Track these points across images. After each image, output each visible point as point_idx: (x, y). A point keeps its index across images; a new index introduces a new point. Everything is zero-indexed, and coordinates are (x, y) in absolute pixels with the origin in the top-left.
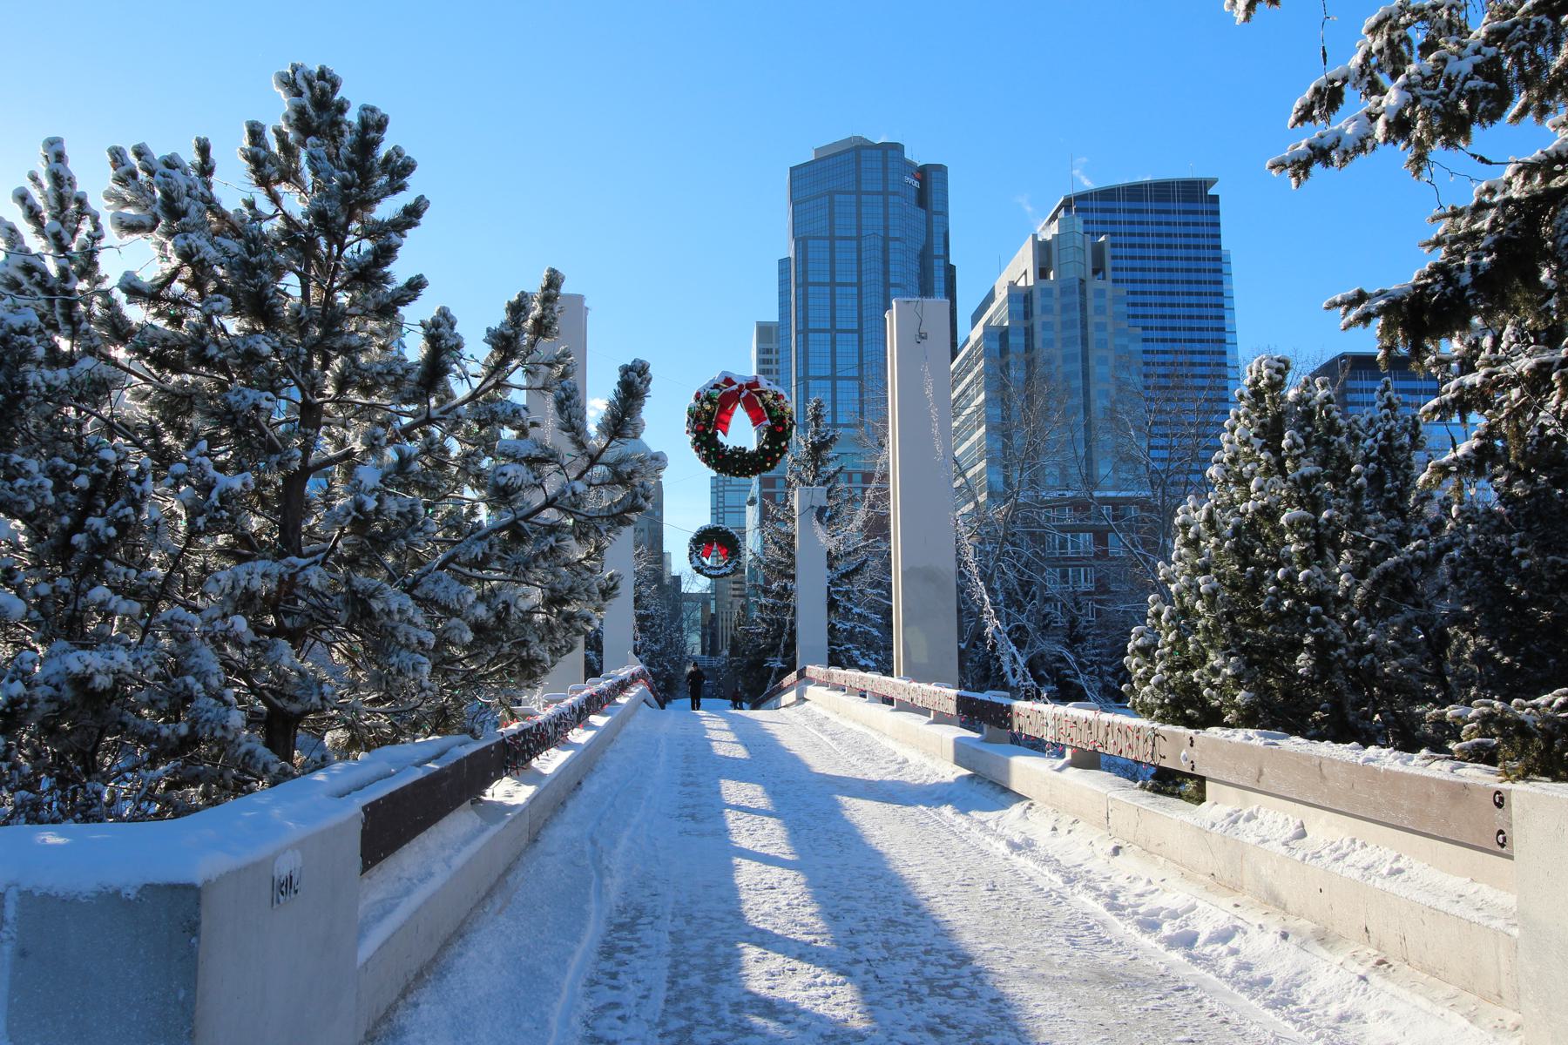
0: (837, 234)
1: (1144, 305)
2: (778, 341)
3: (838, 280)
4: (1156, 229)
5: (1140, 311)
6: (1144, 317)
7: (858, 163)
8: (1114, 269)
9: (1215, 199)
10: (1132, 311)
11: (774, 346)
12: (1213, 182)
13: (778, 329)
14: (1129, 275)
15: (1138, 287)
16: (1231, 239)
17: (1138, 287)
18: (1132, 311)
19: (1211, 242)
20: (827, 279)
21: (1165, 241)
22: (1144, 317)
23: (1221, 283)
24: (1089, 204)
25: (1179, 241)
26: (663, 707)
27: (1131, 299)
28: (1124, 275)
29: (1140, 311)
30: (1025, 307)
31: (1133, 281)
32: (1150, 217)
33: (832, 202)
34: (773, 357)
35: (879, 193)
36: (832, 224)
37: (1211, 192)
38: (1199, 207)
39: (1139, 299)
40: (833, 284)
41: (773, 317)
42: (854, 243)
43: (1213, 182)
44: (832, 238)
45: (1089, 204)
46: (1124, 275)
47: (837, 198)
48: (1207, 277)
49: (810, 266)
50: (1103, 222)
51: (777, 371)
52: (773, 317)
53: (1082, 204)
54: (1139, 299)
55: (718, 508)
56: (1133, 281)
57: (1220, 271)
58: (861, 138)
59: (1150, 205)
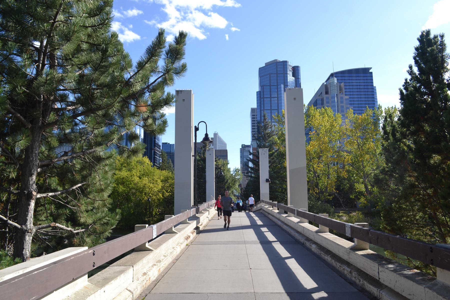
0: (272, 84)
1: (353, 92)
2: (257, 112)
3: (272, 108)
4: (357, 102)
5: (352, 102)
6: (353, 104)
7: (277, 66)
8: (345, 92)
9: (371, 73)
10: (350, 102)
11: (256, 114)
12: (371, 68)
13: (257, 110)
14: (349, 93)
15: (352, 96)
16: (376, 82)
17: (352, 96)
18: (350, 102)
19: (372, 96)
20: (270, 108)
21: (358, 87)
22: (353, 104)
23: (374, 95)
24: (338, 75)
25: (362, 90)
26: (187, 6)
27: (350, 99)
28: (348, 93)
29: (352, 102)
30: (322, 102)
31: (350, 95)
32: (354, 78)
33: (270, 76)
34: (255, 117)
35: (282, 74)
36: (270, 82)
37: (370, 71)
38: (367, 75)
39: (352, 99)
40: (270, 86)
41: (255, 106)
42: (276, 87)
43: (371, 68)
44: (270, 86)
45: (338, 75)
46: (348, 93)
47: (271, 75)
48: (370, 90)
49: (265, 93)
50: (342, 80)
51: (257, 118)
52: (255, 106)
53: (336, 75)
54: (352, 99)
55: (242, 162)
56: (350, 95)
57: (374, 101)
58: (277, 60)
59: (354, 75)
